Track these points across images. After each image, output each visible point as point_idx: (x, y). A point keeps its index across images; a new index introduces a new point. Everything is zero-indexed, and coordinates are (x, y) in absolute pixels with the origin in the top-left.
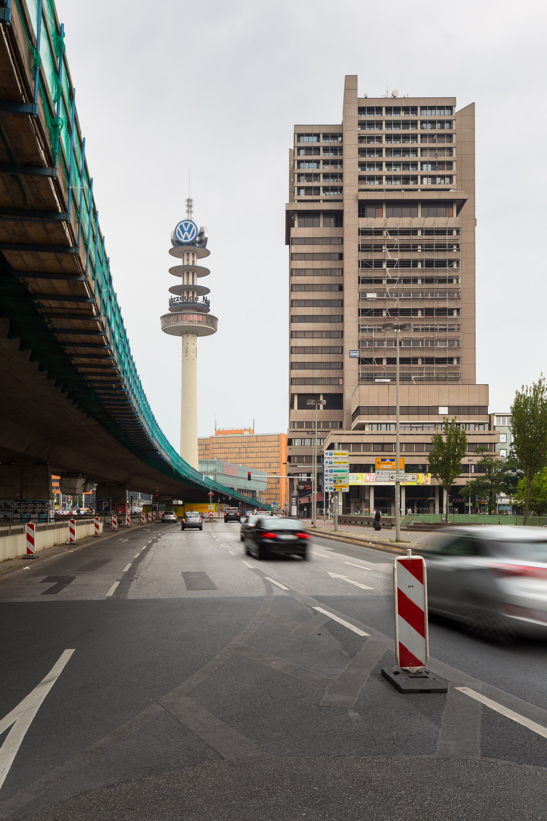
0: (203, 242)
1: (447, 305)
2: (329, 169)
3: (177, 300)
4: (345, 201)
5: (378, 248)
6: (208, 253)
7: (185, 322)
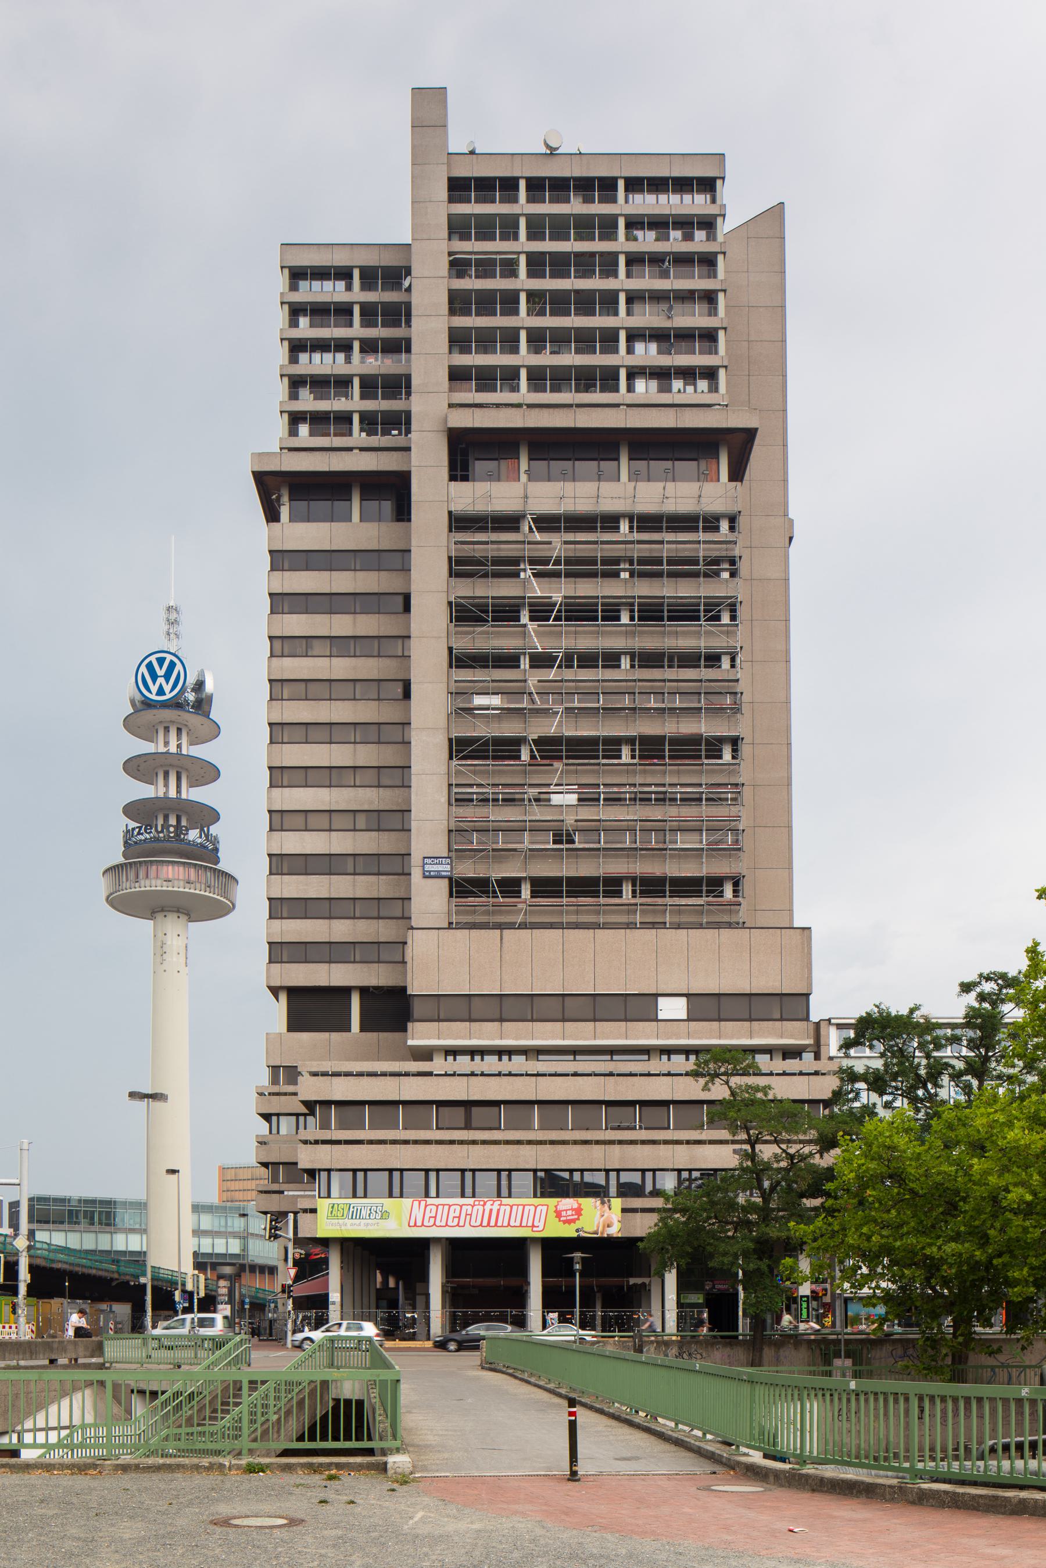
0: (202, 705)
1: (705, 727)
2: (376, 364)
3: (139, 833)
5: (506, 567)
6: (216, 731)
7: (153, 882)
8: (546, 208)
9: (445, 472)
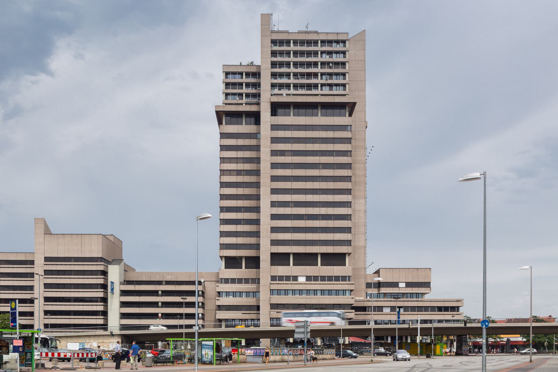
2: (251, 90)
4: (262, 104)
9: (270, 113)
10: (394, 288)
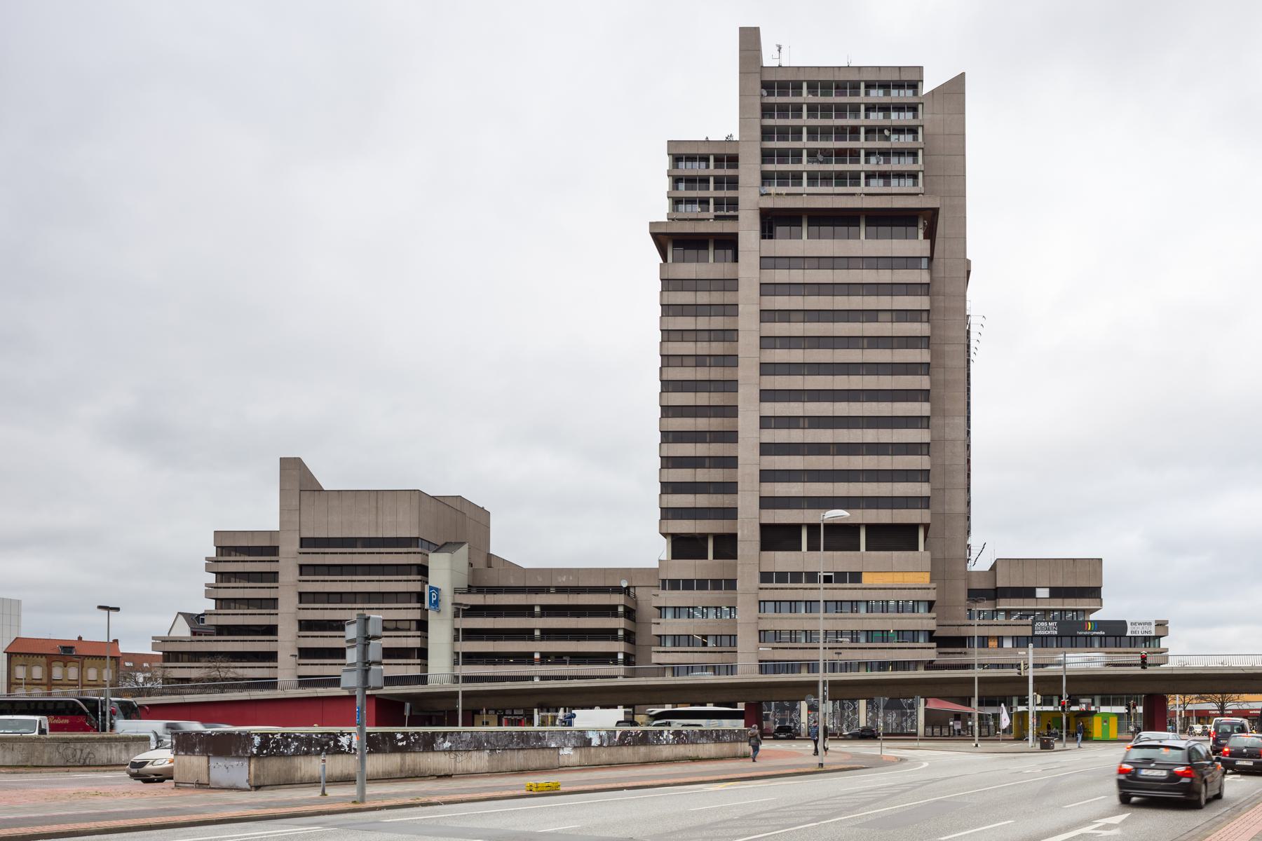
8: (819, 122)
10: (1026, 600)
